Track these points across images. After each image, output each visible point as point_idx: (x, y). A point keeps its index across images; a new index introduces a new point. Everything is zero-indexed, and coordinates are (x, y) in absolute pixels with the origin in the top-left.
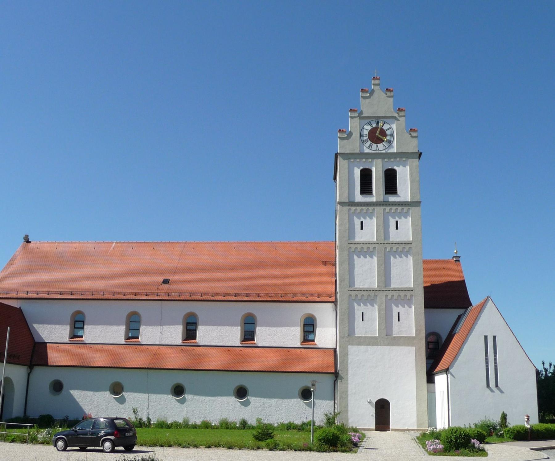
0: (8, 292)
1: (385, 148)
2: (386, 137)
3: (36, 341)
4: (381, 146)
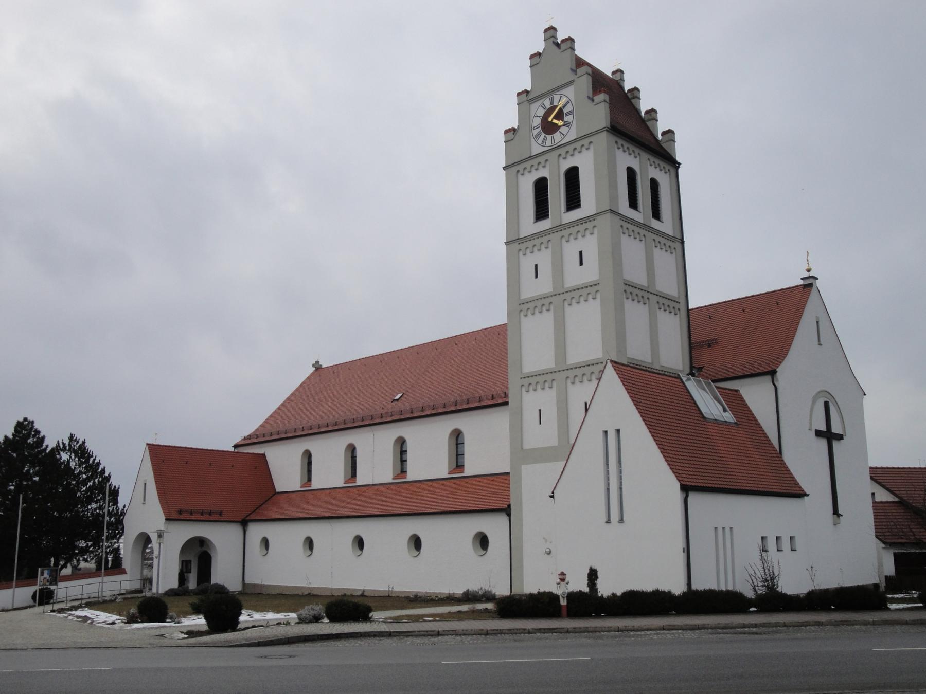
1: (563, 137)
2: (562, 120)
3: (277, 491)
4: (557, 136)
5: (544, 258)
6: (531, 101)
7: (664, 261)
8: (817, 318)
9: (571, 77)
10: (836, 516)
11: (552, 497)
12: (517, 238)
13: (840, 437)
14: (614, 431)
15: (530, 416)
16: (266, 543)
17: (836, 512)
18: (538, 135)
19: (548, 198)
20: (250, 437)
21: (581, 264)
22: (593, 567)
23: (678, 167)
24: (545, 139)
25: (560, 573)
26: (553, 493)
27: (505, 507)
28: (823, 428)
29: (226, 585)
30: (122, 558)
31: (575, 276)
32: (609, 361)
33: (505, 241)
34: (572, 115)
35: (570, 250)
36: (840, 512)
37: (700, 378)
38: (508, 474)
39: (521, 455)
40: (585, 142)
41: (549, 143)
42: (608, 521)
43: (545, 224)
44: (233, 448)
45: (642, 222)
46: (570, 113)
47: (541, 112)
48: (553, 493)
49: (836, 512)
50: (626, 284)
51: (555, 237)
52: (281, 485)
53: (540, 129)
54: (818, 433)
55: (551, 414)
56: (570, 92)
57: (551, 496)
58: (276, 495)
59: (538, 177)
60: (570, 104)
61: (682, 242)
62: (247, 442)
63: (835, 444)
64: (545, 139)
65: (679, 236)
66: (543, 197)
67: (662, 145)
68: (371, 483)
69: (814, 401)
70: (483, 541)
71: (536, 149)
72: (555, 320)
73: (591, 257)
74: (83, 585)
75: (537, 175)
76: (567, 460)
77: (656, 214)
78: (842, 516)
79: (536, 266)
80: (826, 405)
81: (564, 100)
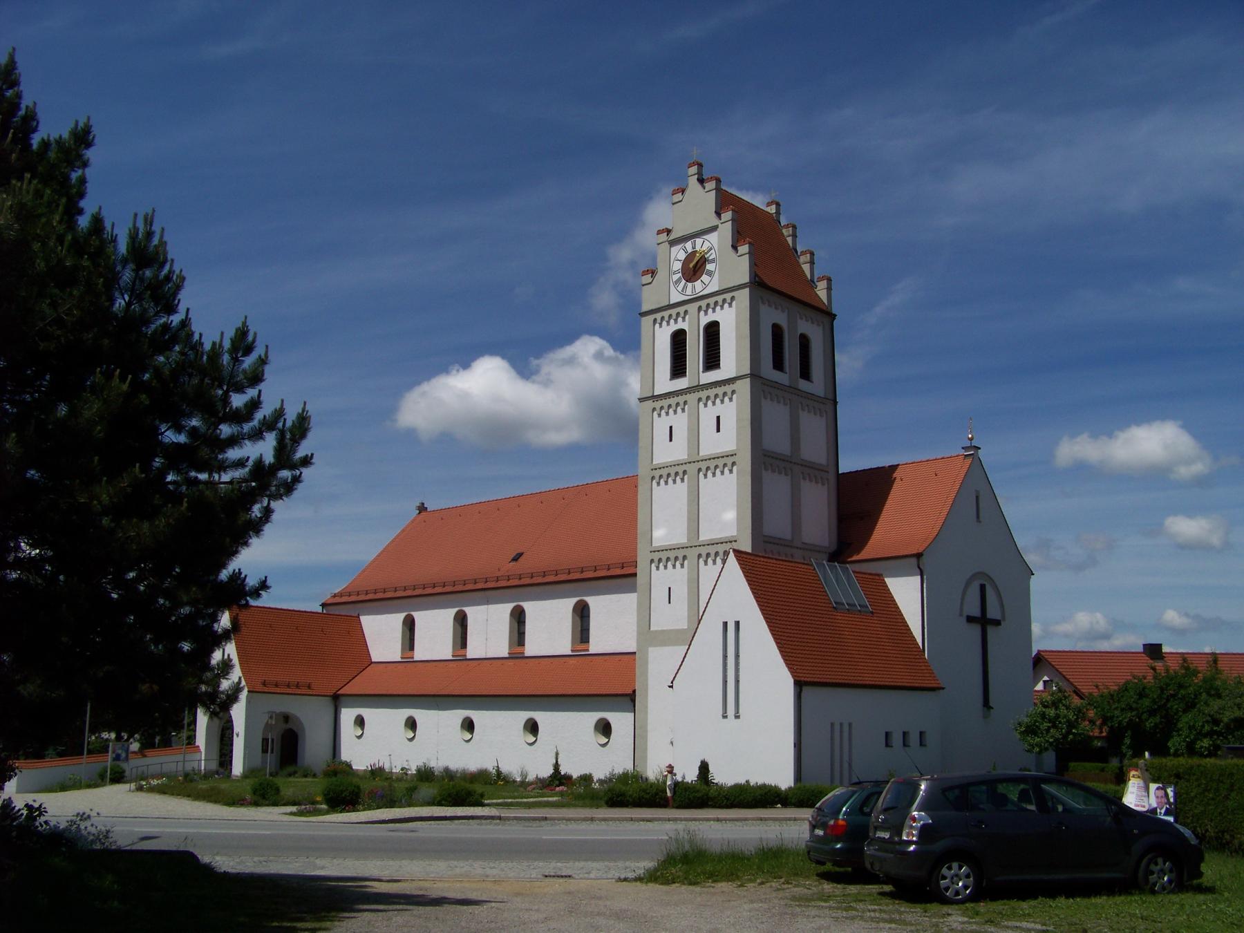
0: (477, 581)
3: (373, 661)
5: (680, 421)
6: (673, 243)
7: (812, 426)
8: (977, 492)
9: (715, 221)
10: (985, 708)
11: (671, 687)
12: (651, 395)
13: (997, 623)
14: (734, 623)
15: (659, 594)
16: (360, 722)
17: (986, 703)
18: (678, 281)
19: (686, 353)
20: (341, 594)
21: (718, 430)
22: (12, 799)
23: (834, 319)
24: (685, 287)
25: (667, 765)
26: (672, 683)
27: (630, 691)
28: (976, 612)
29: (698, 766)
30: (775, 786)
31: (713, 443)
32: (731, 550)
33: (639, 397)
34: (715, 264)
35: (708, 414)
36: (991, 705)
37: (836, 564)
38: (635, 653)
39: (648, 635)
40: (728, 296)
41: (689, 291)
42: (725, 717)
43: (682, 383)
44: (321, 607)
45: (787, 384)
46: (713, 261)
47: (682, 256)
48: (672, 683)
49: (986, 703)
50: (765, 455)
51: (692, 398)
52: (377, 654)
53: (680, 274)
54: (970, 619)
55: (681, 592)
56: (713, 238)
57: (670, 687)
58: (372, 665)
59: (677, 328)
60: (713, 251)
61: (835, 403)
62: (338, 600)
63: (991, 631)
64: (685, 287)
65: (830, 396)
66: (681, 351)
67: (818, 293)
68: (483, 656)
69: (968, 584)
70: (604, 728)
71: (676, 297)
72: (690, 493)
73: (729, 423)
74: (177, 762)
75: (674, 327)
76: (689, 646)
77: (805, 374)
78: (992, 708)
79: (671, 427)
80: (983, 588)
81: (707, 245)
